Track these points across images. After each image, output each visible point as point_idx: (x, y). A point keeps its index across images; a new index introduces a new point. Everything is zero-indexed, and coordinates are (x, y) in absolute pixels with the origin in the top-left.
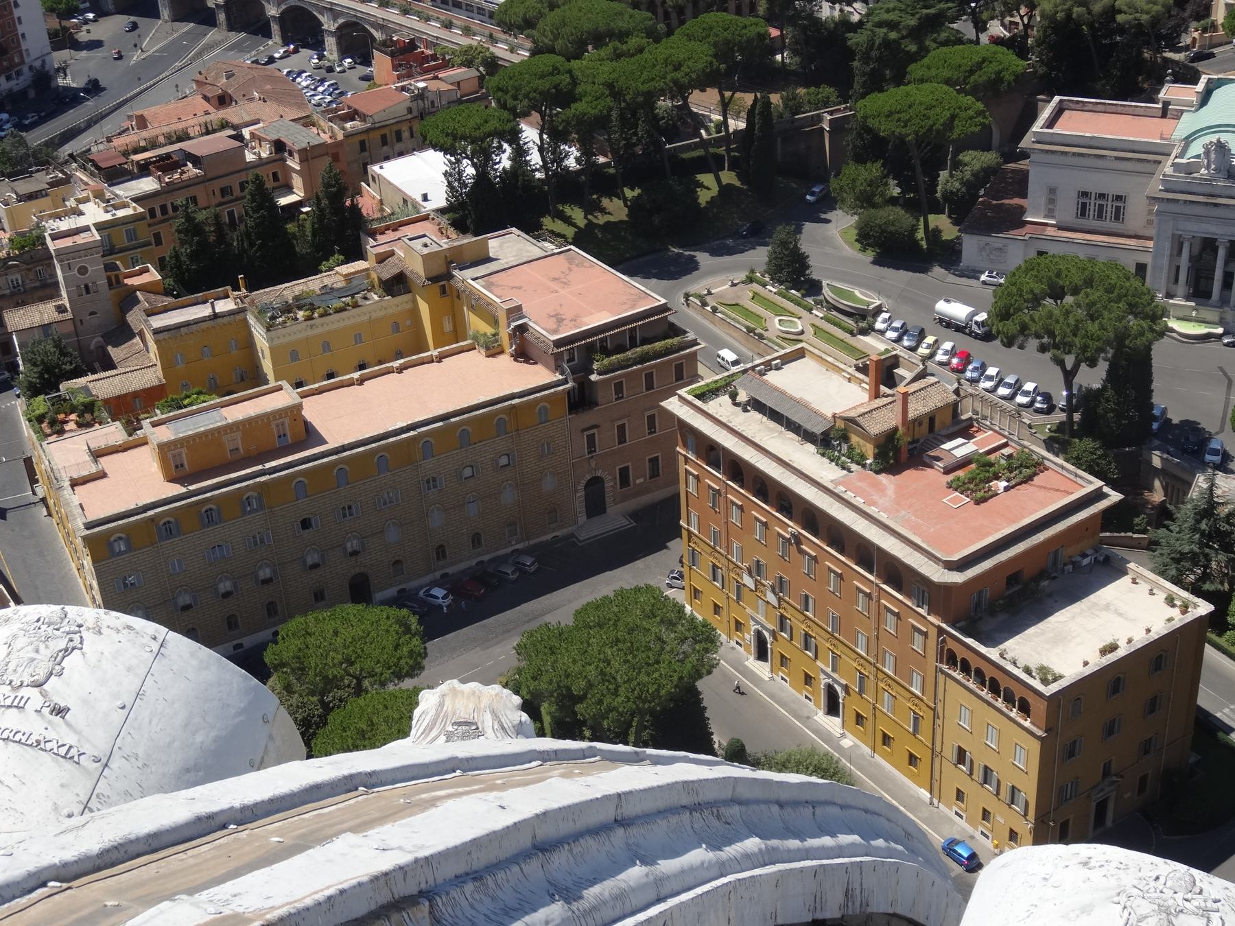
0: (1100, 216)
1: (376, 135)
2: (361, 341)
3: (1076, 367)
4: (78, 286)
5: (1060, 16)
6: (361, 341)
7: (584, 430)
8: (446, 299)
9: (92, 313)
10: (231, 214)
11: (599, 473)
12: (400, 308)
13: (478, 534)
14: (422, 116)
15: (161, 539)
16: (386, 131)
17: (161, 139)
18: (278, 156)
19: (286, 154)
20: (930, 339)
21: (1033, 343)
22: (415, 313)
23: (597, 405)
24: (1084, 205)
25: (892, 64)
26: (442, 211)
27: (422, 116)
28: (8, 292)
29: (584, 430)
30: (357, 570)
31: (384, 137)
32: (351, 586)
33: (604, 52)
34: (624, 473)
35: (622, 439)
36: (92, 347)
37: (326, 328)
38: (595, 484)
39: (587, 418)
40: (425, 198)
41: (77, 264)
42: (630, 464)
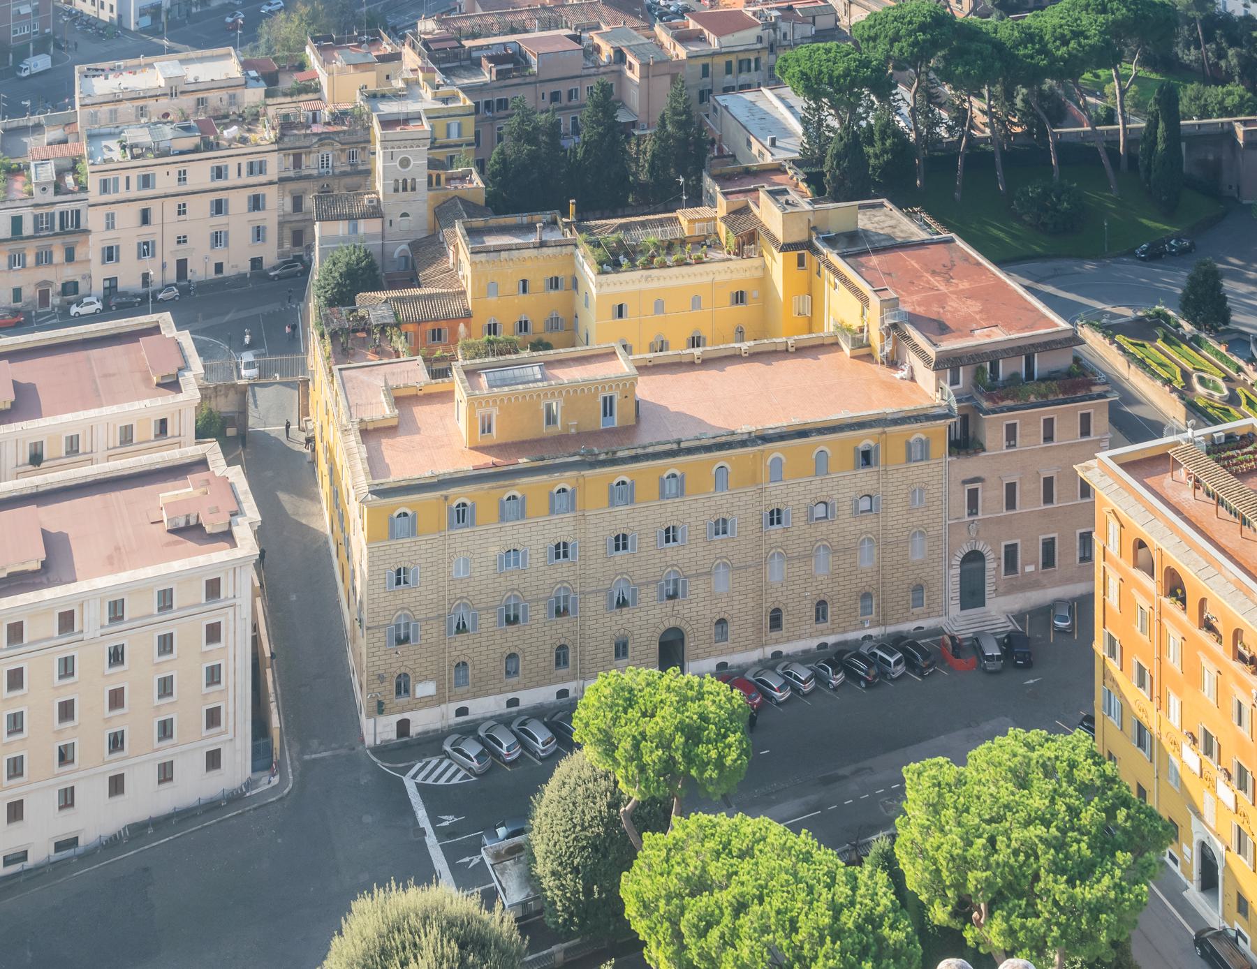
1: (721, 62)
2: (700, 307)
4: (397, 181)
6: (700, 307)
7: (965, 482)
8: (803, 274)
9: (405, 215)
12: (748, 274)
13: (406, 675)
14: (772, 48)
15: (451, 527)
16: (732, 58)
17: (496, 29)
18: (615, 67)
19: (626, 67)
22: (764, 279)
23: (984, 450)
27: (772, 48)
28: (315, 172)
29: (965, 482)
30: (672, 623)
31: (729, 64)
32: (660, 644)
34: (1011, 551)
35: (1011, 504)
36: (396, 256)
37: (662, 284)
38: (974, 559)
39: (970, 466)
41: (401, 154)
42: (1018, 541)
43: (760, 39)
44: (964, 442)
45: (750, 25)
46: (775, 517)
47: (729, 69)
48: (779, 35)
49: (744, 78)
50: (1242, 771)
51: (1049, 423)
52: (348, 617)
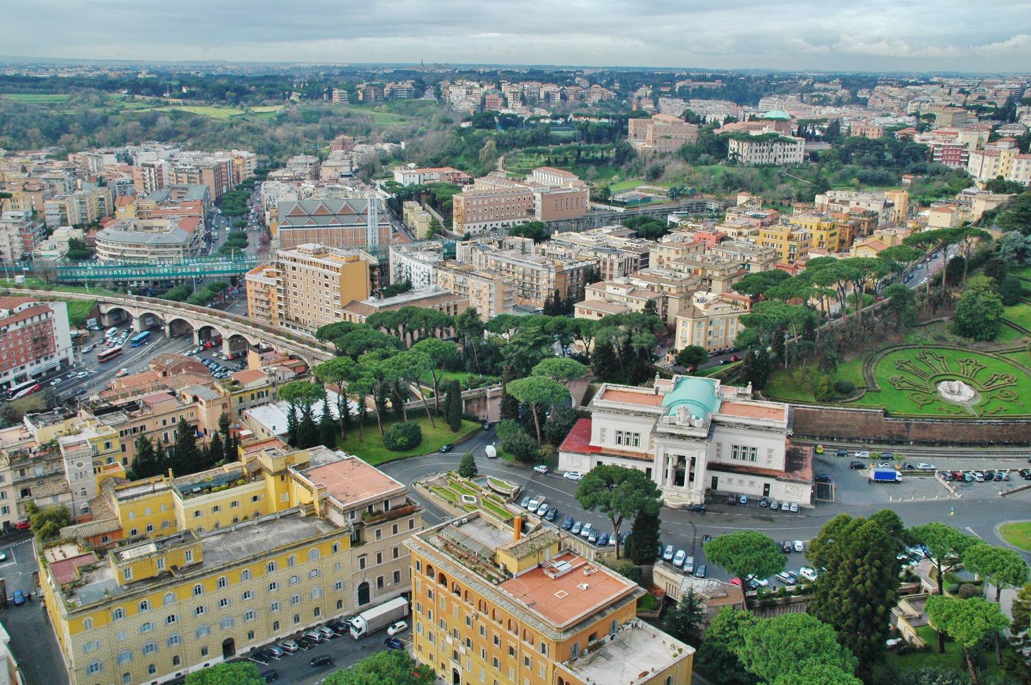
0: (744, 458)
3: (620, 520)
5: (605, 342)
10: (166, 435)
11: (366, 580)
19: (814, 314)
20: (578, 524)
21: (598, 508)
22: (265, 491)
24: (735, 453)
25: (524, 366)
26: (283, 435)
30: (228, 637)
31: (253, 396)
33: (375, 353)
34: (380, 581)
39: (360, 550)
40: (274, 428)
43: (267, 382)
44: (357, 542)
45: (263, 375)
46: (272, 586)
47: (253, 397)
48: (277, 378)
49: (261, 400)
50: (468, 640)
51: (395, 527)
52: (67, 666)
